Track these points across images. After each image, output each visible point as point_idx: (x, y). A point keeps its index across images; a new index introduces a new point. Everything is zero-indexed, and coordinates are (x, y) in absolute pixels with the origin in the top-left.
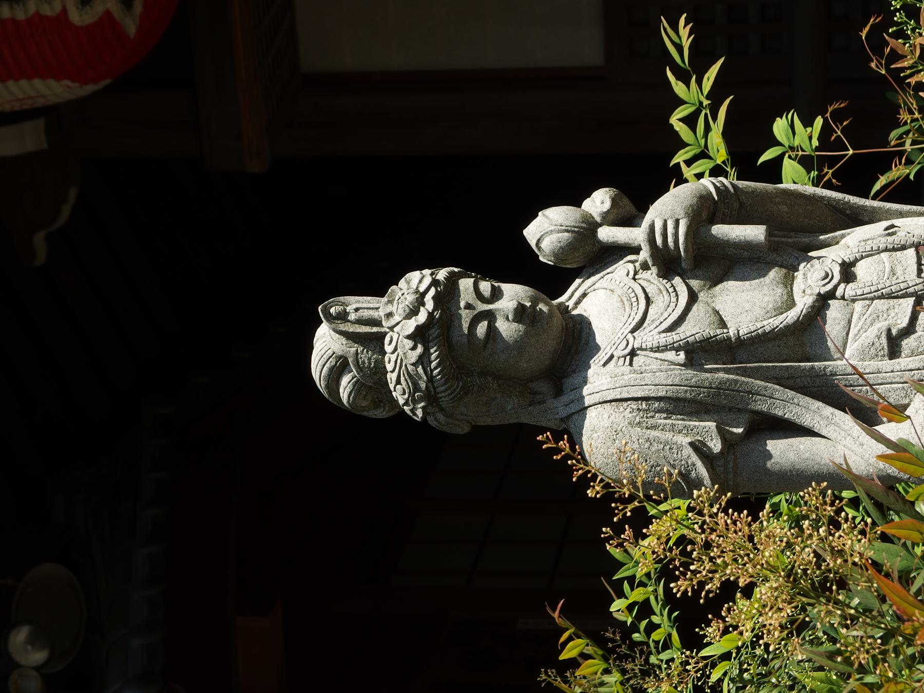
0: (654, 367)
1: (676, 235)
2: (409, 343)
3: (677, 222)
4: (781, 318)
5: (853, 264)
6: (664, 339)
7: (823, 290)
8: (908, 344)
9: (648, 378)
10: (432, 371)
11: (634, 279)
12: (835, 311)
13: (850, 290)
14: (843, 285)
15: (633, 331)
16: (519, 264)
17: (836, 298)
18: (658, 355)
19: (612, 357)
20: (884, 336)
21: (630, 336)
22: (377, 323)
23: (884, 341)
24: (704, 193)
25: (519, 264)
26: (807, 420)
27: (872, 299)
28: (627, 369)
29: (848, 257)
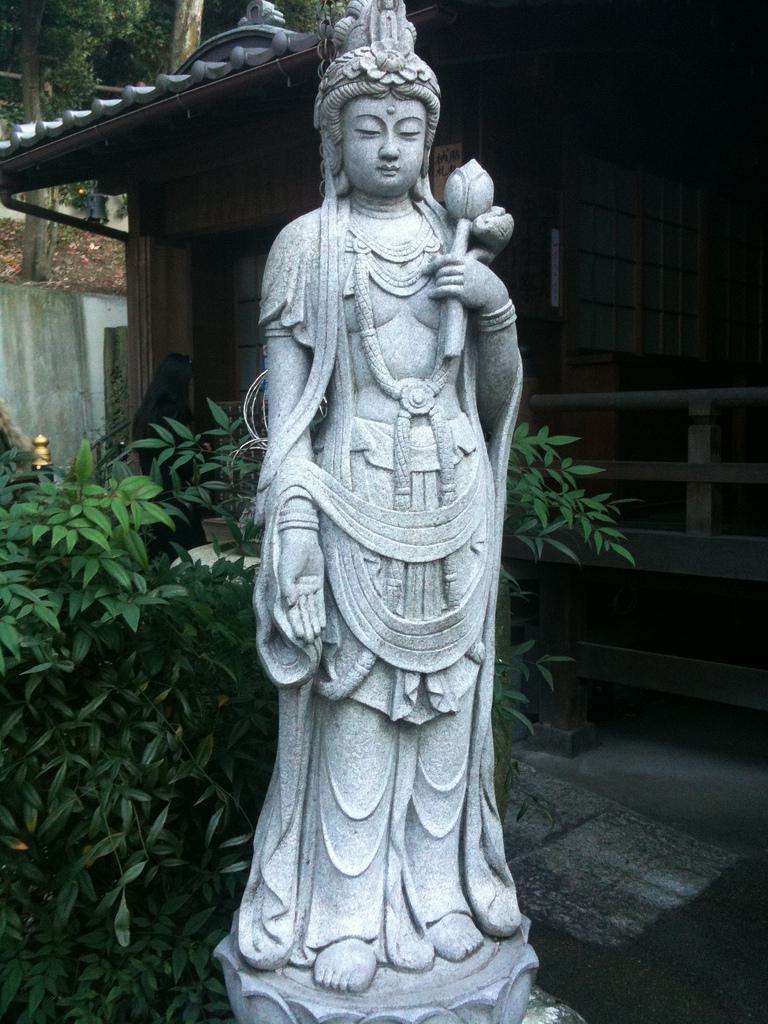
0: (343, 270)
1: (450, 283)
2: (355, 66)
3: (461, 283)
4: (385, 370)
5: (430, 423)
6: (363, 276)
7: (405, 402)
8: (360, 465)
9: (333, 266)
10: (338, 88)
11: (424, 252)
12: (391, 407)
13: (404, 421)
14: (409, 415)
15: (373, 252)
16: (439, 167)
17: (8, 614)
18: (351, 273)
19: (355, 237)
20: (365, 447)
21: (369, 250)
22: (378, 38)
23: (362, 447)
24: (355, 214)
25: (439, 167)
26: (309, 391)
27: (394, 438)
28: (341, 249)
29: (436, 418)
